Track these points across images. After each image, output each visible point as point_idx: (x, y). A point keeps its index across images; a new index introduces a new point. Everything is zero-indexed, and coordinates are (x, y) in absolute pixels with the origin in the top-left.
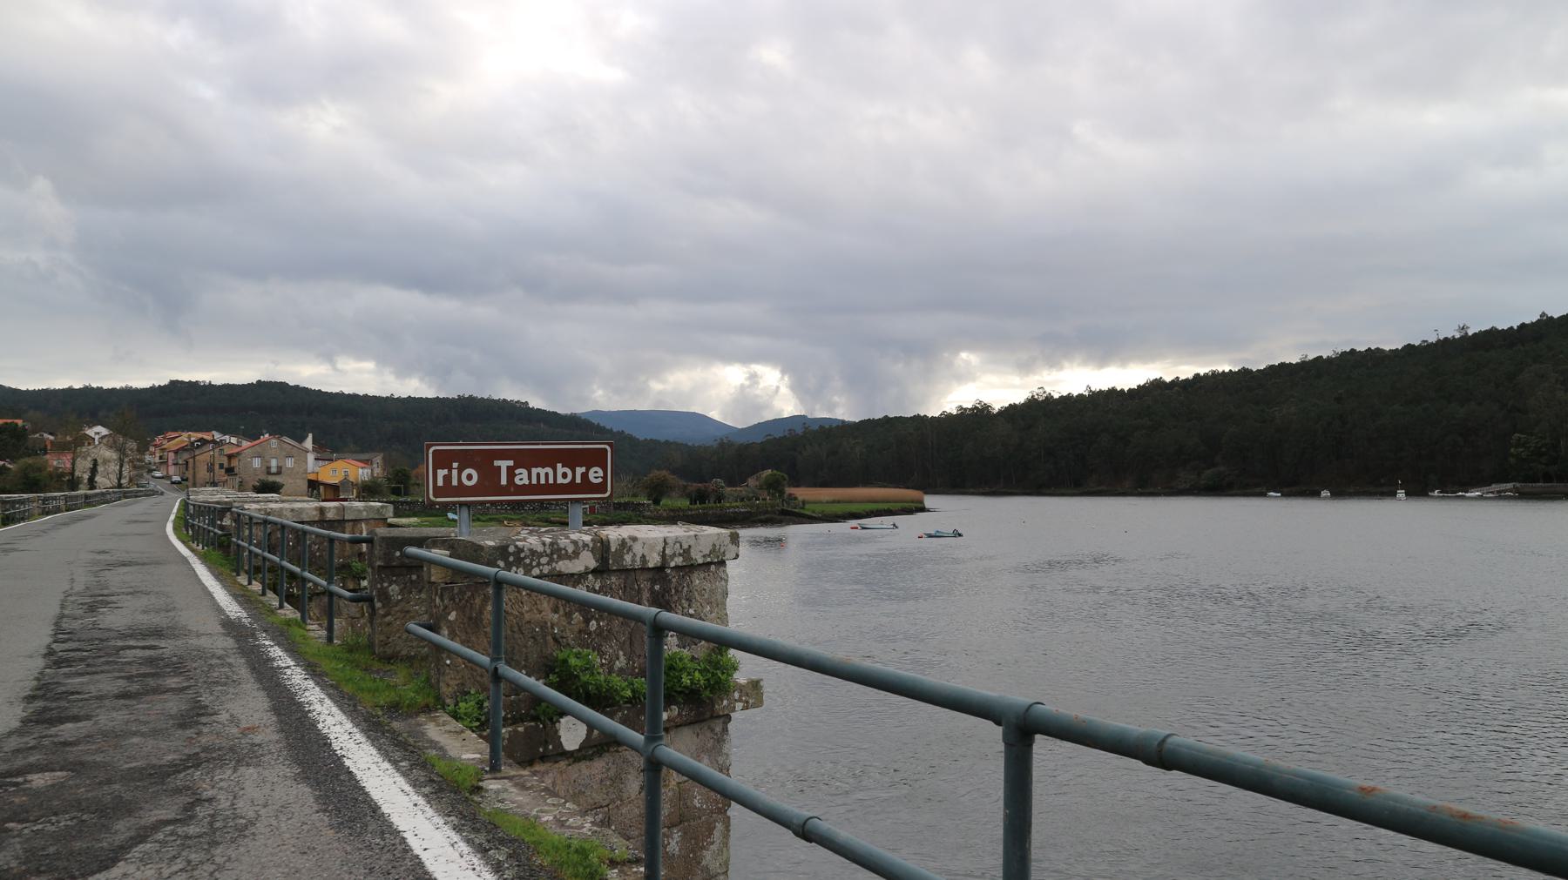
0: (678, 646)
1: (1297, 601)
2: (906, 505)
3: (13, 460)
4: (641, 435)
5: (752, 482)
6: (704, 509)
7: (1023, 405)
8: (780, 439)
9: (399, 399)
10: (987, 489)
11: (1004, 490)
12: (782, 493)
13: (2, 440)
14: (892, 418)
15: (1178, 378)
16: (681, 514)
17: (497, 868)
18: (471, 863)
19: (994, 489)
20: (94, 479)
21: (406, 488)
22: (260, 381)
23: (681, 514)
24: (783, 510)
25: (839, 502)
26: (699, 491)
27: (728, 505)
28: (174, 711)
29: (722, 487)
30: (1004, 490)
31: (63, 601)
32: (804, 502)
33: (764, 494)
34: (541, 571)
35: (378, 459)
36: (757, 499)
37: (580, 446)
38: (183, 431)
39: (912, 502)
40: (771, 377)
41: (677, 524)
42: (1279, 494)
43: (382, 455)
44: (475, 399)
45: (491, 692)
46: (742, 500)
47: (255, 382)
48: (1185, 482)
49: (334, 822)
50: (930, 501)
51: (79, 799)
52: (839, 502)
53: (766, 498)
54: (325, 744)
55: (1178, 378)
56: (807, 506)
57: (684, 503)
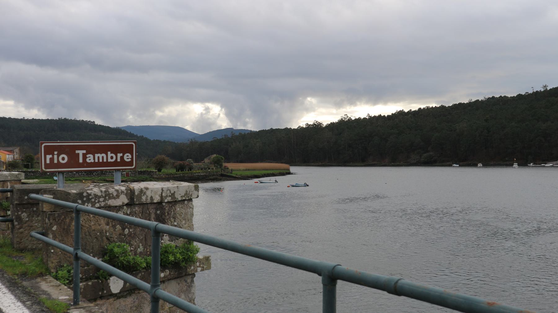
0: (169, 240)
2: (281, 171)
4: (152, 137)
5: (206, 160)
6: (183, 174)
8: (220, 139)
10: (362, 164)
12: (221, 165)
14: (274, 130)
16: (172, 176)
19: (323, 164)
21: (32, 165)
23: (172, 176)
24: (222, 174)
25: (249, 170)
26: (180, 165)
27: (195, 172)
32: (232, 170)
33: (212, 166)
35: (17, 150)
36: (209, 169)
43: (19, 148)
46: (202, 169)
48: (414, 160)
50: (293, 169)
52: (249, 170)
53: (214, 169)
55: (411, 110)
56: (233, 172)
57: (173, 171)
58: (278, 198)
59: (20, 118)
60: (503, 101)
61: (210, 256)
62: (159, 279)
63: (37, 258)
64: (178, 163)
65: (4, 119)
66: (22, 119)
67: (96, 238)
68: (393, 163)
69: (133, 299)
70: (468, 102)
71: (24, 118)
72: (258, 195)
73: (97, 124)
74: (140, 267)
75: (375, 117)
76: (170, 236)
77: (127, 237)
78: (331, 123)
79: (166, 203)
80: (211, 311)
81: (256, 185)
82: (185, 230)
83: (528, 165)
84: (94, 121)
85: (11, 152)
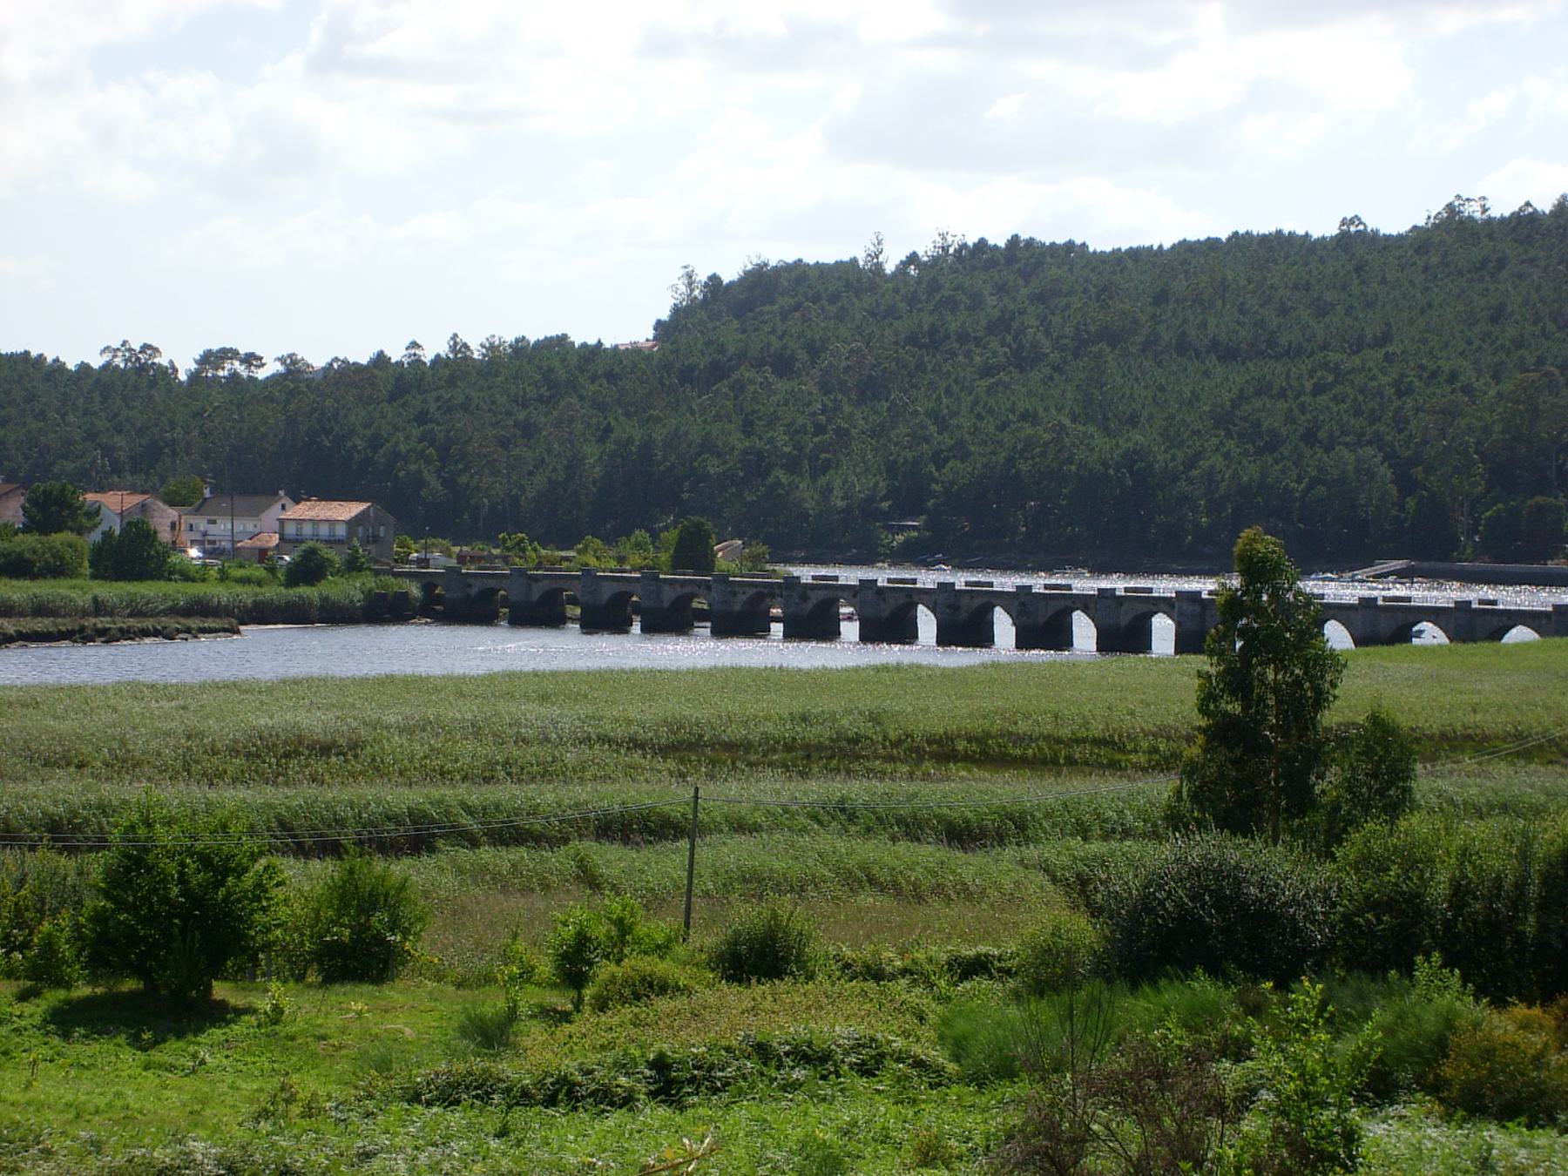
0: (23, 997)
1: (963, 405)
3: (234, 375)
7: (1101, 257)
9: (593, 353)
11: (1479, 565)
13: (1238, 1170)
15: (1237, 233)
17: (4, 687)
18: (236, 1109)
20: (242, 1014)
22: (1377, 231)
28: (61, 997)
29: (1319, 832)
30: (1479, 565)
31: (334, 744)
34: (244, 527)
37: (901, 586)
38: (1521, 1001)
39: (185, 768)
40: (780, 611)
41: (1456, 603)
42: (731, 579)
44: (551, 338)
45: (1421, 594)
47: (1224, 237)
49: (1553, 859)
51: (1413, 391)
54: (153, 383)
56: (1426, 782)
58: (1123, 396)
59: (1395, 233)
60: (1279, 246)
61: (455, 336)
62: (1447, 595)
63: (682, 775)
64: (130, 1113)
65: (23, 367)
66: (1217, 240)
67: (620, 923)
68: (1252, 1016)
69: (290, 1107)
70: (96, 362)
71: (414, 345)
72: (1067, 1025)
73: (458, 346)
74: (305, 970)
75: (1375, 233)
76: (322, 372)
77: (1456, 505)
78: (1247, 233)
79: (1248, 665)
80: (587, 1042)
81: (528, 640)
82: (607, 788)
83: (221, 990)
84: (26, 351)
85: (705, 367)
